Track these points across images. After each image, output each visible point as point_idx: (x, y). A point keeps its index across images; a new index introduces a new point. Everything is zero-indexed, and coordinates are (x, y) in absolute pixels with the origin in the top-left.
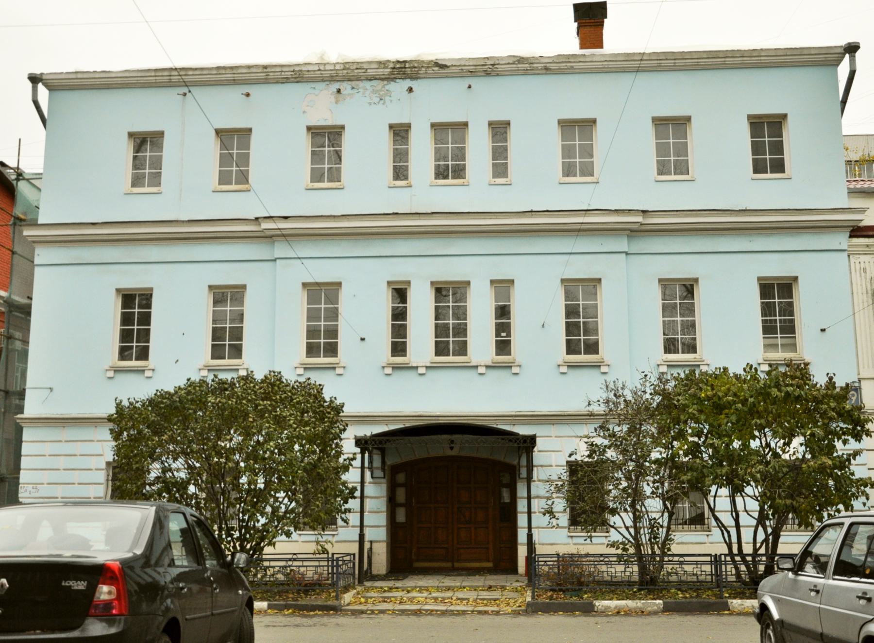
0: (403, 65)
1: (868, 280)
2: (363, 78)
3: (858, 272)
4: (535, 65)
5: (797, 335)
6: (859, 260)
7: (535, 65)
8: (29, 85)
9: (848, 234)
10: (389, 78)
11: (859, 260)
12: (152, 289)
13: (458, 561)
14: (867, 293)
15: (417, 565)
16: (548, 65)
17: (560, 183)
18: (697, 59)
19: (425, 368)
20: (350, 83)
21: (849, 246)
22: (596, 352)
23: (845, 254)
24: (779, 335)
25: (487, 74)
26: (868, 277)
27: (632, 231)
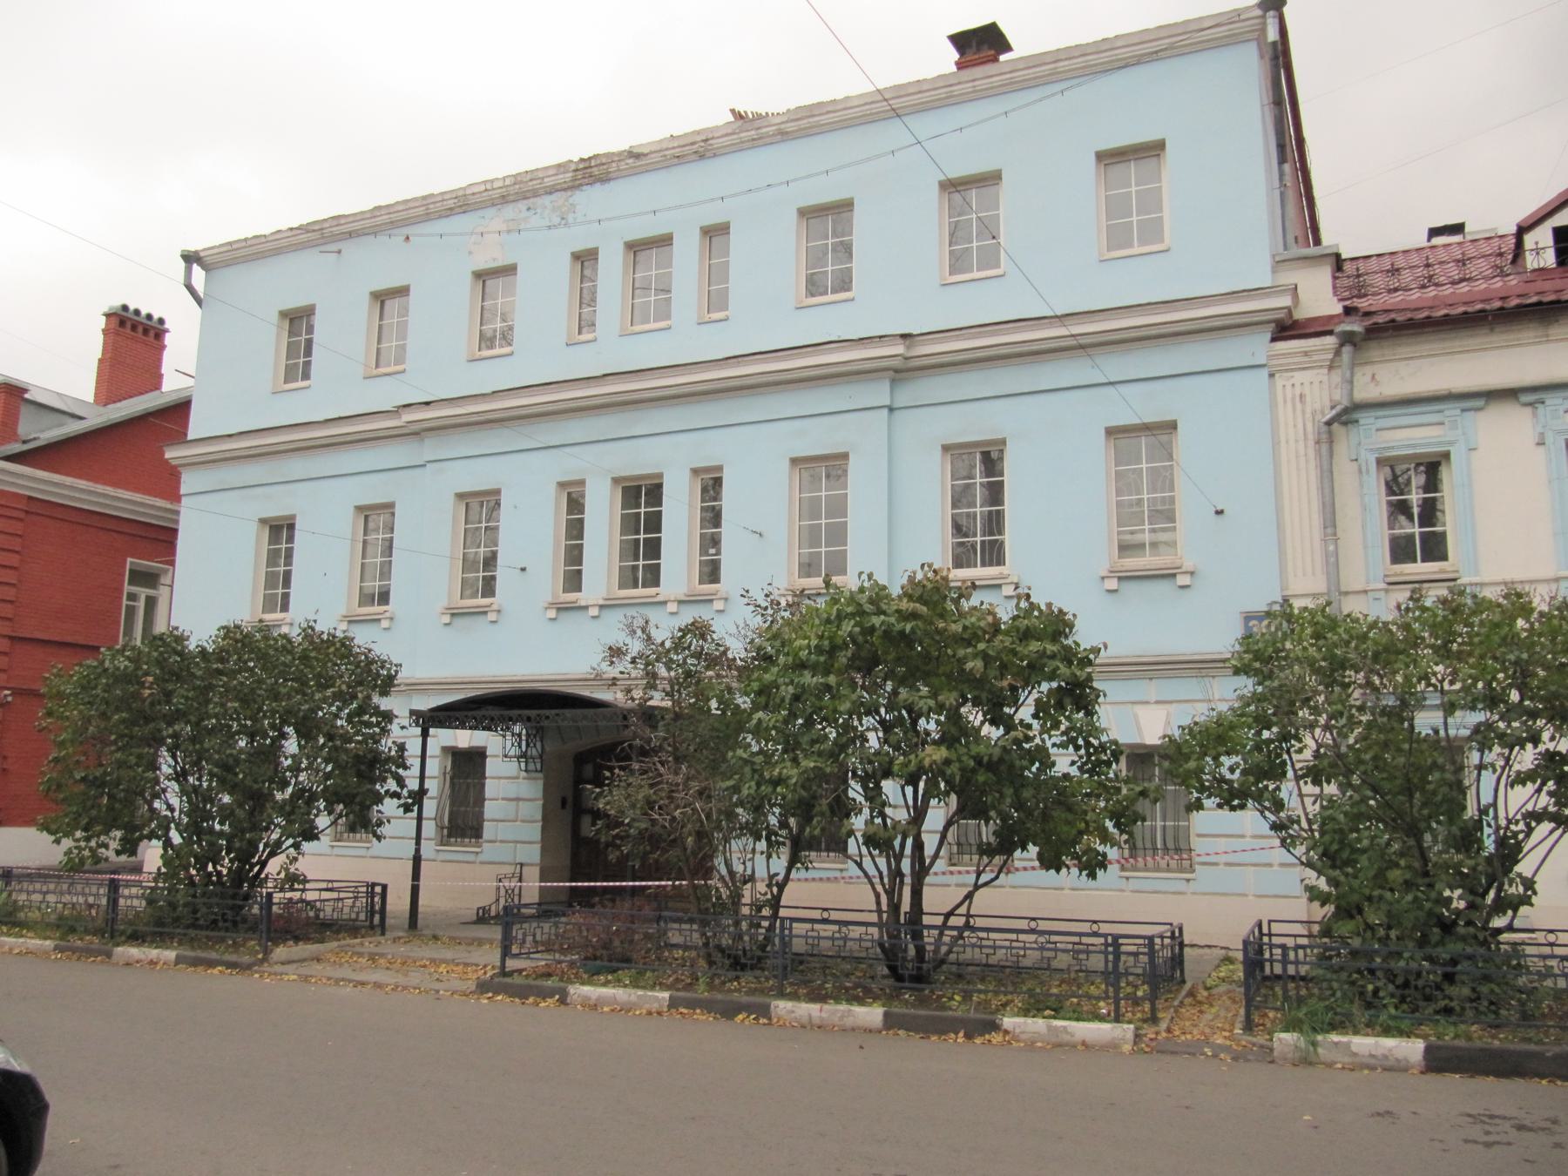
0: (587, 164)
1: (1308, 415)
2: (541, 192)
3: (1289, 405)
4: (764, 130)
6: (1291, 382)
7: (764, 130)
8: (182, 264)
9: (1269, 336)
11: (1291, 382)
12: (660, 476)
14: (1306, 438)
16: (783, 126)
18: (1011, 72)
19: (676, 604)
20: (525, 202)
21: (1270, 357)
22: (1000, 561)
23: (1265, 373)
24: (1147, 527)
25: (701, 156)
26: (1308, 410)
27: (896, 371)
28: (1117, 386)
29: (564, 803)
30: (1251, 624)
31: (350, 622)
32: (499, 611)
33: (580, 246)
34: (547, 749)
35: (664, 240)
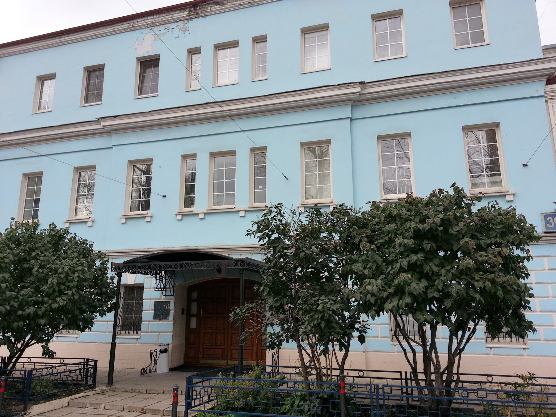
2: (172, 21)
5: (501, 172)
9: (545, 82)
10: (188, 19)
13: (231, 359)
15: (202, 361)
17: (302, 74)
20: (164, 26)
21: (546, 92)
28: (245, 132)
29: (183, 311)
30: (548, 219)
31: (70, 223)
32: (151, 217)
33: (192, 46)
34: (177, 284)
35: (235, 44)
